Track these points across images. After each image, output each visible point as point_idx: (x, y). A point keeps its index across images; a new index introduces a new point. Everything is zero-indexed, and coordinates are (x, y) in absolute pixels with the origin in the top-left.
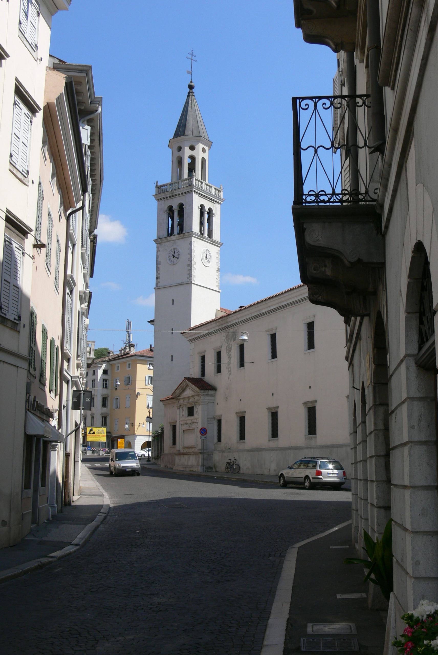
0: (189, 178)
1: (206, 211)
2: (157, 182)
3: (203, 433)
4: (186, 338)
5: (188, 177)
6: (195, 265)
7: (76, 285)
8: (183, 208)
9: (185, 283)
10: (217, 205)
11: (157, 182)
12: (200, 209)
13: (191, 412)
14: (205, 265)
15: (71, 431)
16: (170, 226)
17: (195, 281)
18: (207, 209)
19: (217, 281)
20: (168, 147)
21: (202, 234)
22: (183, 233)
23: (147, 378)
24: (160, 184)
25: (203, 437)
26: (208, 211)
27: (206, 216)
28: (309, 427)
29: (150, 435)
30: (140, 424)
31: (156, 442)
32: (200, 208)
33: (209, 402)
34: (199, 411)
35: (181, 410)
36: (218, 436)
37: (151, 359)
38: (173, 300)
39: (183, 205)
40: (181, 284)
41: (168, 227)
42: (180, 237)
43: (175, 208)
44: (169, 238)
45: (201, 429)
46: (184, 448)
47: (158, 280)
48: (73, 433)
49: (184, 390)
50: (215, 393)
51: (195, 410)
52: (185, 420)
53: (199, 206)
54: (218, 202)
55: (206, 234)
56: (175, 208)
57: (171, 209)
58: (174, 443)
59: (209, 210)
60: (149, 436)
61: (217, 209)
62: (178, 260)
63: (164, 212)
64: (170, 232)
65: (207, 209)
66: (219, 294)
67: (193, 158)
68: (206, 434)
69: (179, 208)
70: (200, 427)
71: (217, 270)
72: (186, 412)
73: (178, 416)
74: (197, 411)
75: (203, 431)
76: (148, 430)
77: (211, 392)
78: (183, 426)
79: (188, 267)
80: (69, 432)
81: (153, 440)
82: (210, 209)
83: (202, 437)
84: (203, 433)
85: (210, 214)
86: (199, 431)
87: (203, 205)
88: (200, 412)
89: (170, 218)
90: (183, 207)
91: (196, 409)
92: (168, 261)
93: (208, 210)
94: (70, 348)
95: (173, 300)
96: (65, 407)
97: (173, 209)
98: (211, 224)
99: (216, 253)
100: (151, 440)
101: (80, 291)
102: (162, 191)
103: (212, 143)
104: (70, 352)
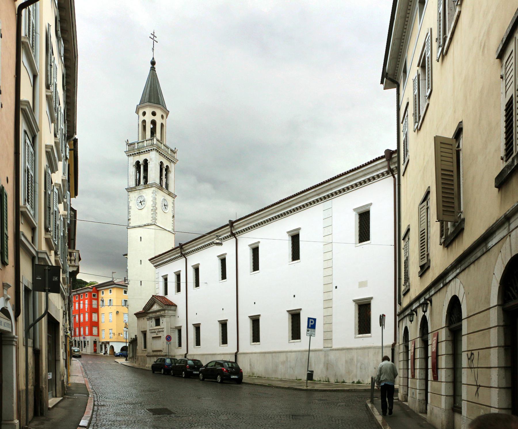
0: (152, 138)
1: (164, 167)
2: (128, 140)
3: (169, 337)
4: (153, 264)
5: (151, 137)
6: (157, 210)
7: (39, 131)
8: (148, 163)
9: (150, 224)
10: (172, 164)
11: (128, 140)
12: (160, 165)
13: (158, 323)
14: (165, 212)
15: (40, 316)
16: (138, 178)
17: (156, 223)
18: (165, 166)
19: (173, 225)
20: (135, 113)
21: (162, 186)
22: (148, 183)
23: (123, 301)
24: (130, 142)
25: (168, 342)
26: (166, 168)
27: (164, 172)
28: (223, 339)
29: (127, 342)
30: (119, 333)
31: (131, 346)
32: (160, 164)
33: (171, 315)
34: (164, 322)
35: (150, 321)
36: (178, 342)
37: (125, 288)
38: (141, 237)
39: (148, 161)
40: (147, 225)
41: (136, 179)
42: (146, 186)
43: (141, 162)
44: (138, 188)
45: (167, 336)
46: (153, 351)
47: (130, 221)
48: (43, 319)
49: (152, 306)
50: (176, 309)
51: (161, 321)
52: (94, 407)
53: (160, 162)
54: (173, 162)
55: (164, 186)
56: (141, 162)
57: (138, 163)
58: (145, 347)
59: (166, 167)
60: (126, 342)
61: (172, 167)
62: (145, 203)
63: (133, 166)
64: (138, 183)
65: (165, 166)
66: (173, 235)
67: (154, 122)
68: (171, 340)
69: (145, 163)
70: (165, 336)
71: (173, 217)
72: (154, 322)
73: (148, 326)
74: (163, 322)
75: (169, 338)
76: (125, 338)
77: (173, 308)
78: (152, 334)
79: (151, 211)
80: (38, 317)
81: (129, 345)
82: (167, 166)
83: (167, 343)
84: (169, 337)
85: (167, 171)
86: (165, 338)
87: (162, 162)
88: (165, 323)
89: (137, 171)
90: (148, 162)
91: (162, 321)
92: (137, 206)
93: (165, 166)
94: (34, 214)
95: (141, 237)
96: (31, 290)
97: (140, 164)
98: (168, 179)
99: (171, 203)
100: (127, 345)
101: (46, 145)
102: (131, 149)
103: (169, 111)
104: (34, 220)
